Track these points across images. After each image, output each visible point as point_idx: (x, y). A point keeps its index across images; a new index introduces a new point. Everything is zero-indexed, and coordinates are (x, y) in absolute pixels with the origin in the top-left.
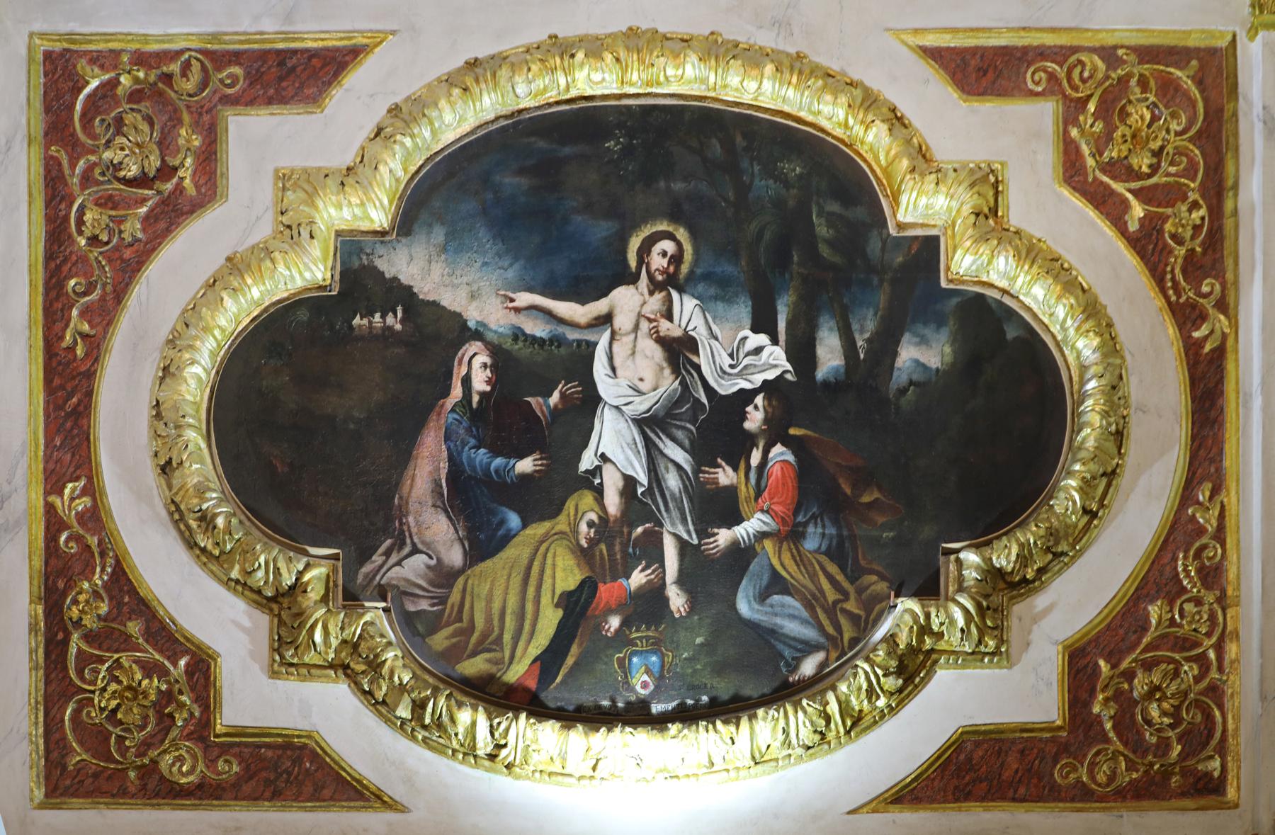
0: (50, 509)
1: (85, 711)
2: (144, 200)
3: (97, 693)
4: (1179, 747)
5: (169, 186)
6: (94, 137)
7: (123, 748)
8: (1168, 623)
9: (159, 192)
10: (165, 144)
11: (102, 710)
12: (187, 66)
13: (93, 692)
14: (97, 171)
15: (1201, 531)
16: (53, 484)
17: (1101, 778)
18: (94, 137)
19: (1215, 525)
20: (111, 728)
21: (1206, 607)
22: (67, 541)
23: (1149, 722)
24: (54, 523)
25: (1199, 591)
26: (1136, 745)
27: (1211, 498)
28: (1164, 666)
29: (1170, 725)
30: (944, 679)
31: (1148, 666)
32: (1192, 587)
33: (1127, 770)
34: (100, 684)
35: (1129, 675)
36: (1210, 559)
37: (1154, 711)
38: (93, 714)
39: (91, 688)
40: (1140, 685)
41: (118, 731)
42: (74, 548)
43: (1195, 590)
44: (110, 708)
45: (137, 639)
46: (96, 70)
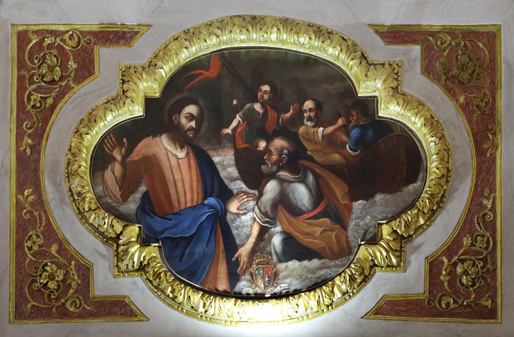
0: (18, 201)
1: (34, 285)
2: (56, 88)
3: (38, 277)
4: (475, 295)
5: (64, 84)
6: (33, 63)
7: (51, 299)
8: (470, 244)
9: (60, 86)
10: (452, 273)
11: (41, 283)
12: (71, 37)
13: (37, 276)
14: (35, 78)
15: (485, 207)
16: (20, 188)
17: (444, 306)
18: (33, 63)
19: (490, 206)
20: (45, 291)
21: (486, 239)
22: (25, 214)
23: (462, 284)
24: (19, 207)
25: (483, 232)
26: (456, 293)
27: (489, 194)
28: (468, 262)
29: (471, 286)
30: (379, 274)
31: (462, 261)
32: (481, 230)
33: (453, 303)
34: (39, 273)
35: (455, 265)
36: (488, 219)
37: (464, 280)
38: (37, 286)
39: (36, 275)
40: (459, 270)
41: (47, 292)
42: (27, 215)
43: (482, 231)
44: (44, 283)
45: (48, 60)
46: (35, 36)
